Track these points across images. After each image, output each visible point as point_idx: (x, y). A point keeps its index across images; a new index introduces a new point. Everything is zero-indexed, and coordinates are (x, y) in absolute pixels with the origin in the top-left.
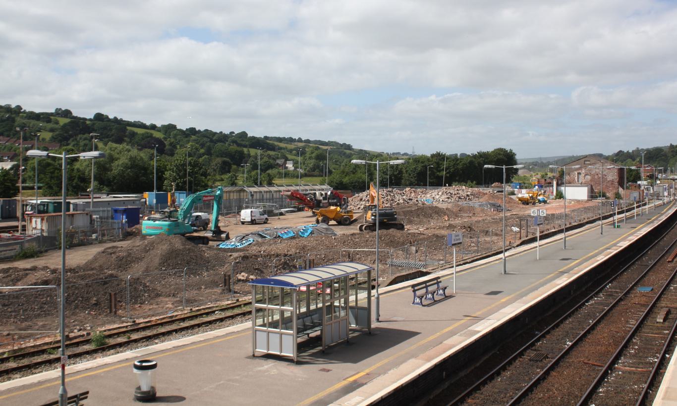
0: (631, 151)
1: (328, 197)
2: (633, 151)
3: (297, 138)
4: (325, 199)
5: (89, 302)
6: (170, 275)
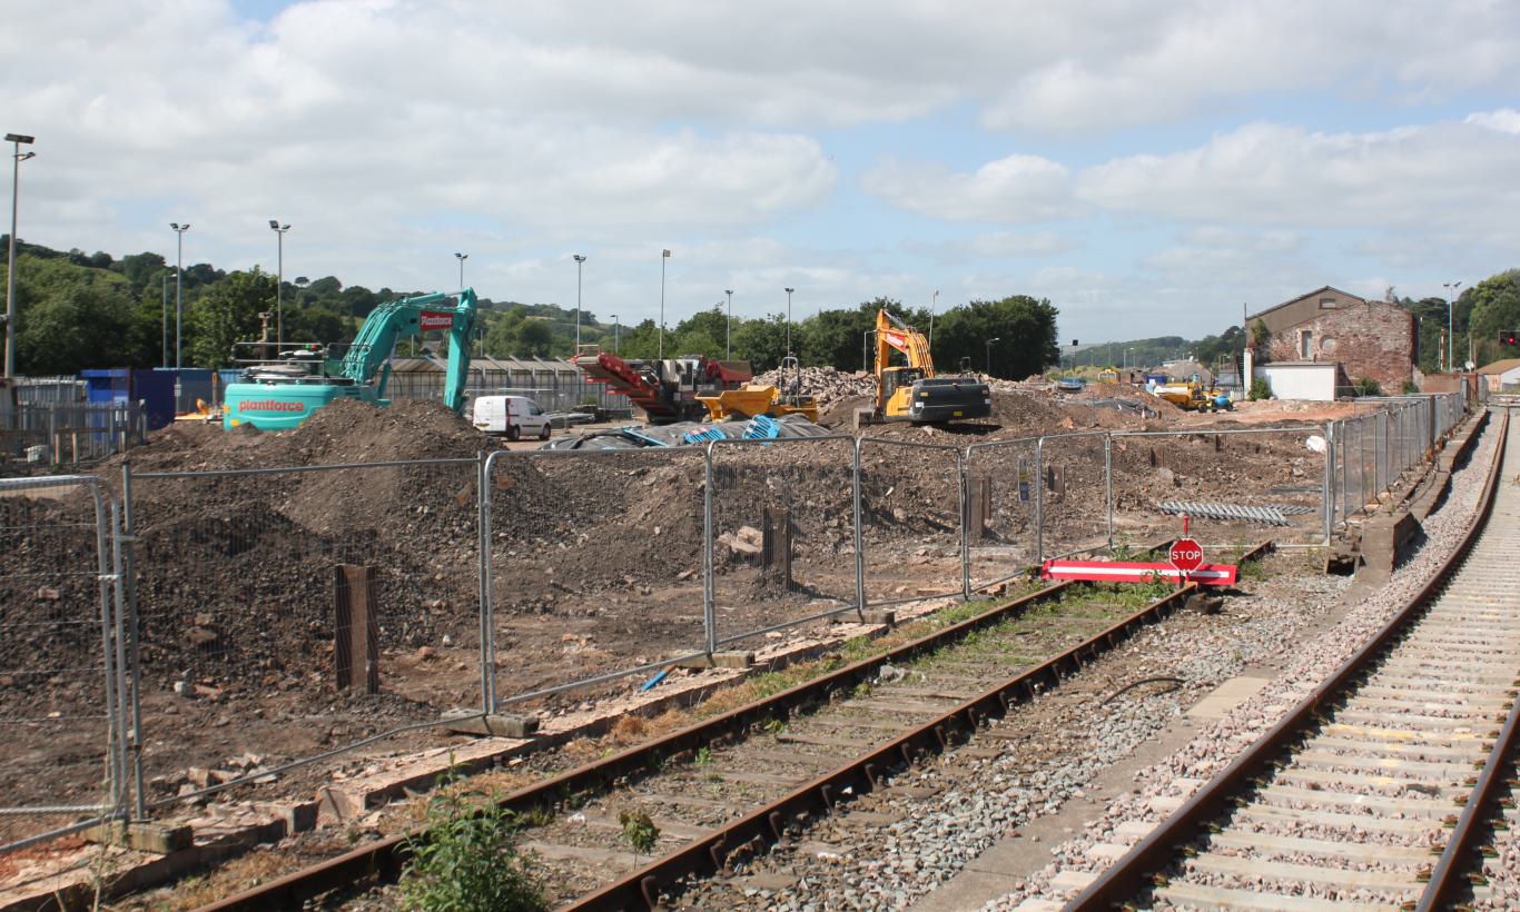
1: (694, 375)
4: (686, 380)
5: (174, 632)
6: (455, 536)
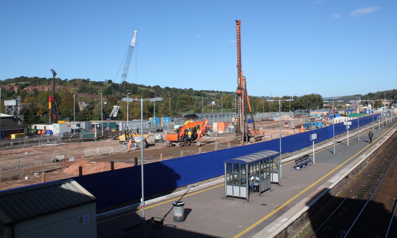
0: (374, 93)
2: (376, 93)
3: (216, 91)
